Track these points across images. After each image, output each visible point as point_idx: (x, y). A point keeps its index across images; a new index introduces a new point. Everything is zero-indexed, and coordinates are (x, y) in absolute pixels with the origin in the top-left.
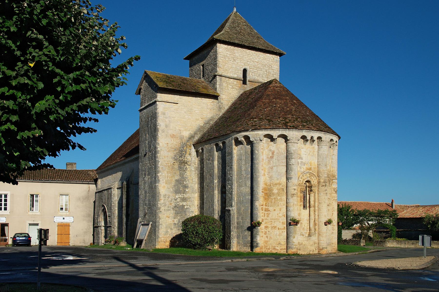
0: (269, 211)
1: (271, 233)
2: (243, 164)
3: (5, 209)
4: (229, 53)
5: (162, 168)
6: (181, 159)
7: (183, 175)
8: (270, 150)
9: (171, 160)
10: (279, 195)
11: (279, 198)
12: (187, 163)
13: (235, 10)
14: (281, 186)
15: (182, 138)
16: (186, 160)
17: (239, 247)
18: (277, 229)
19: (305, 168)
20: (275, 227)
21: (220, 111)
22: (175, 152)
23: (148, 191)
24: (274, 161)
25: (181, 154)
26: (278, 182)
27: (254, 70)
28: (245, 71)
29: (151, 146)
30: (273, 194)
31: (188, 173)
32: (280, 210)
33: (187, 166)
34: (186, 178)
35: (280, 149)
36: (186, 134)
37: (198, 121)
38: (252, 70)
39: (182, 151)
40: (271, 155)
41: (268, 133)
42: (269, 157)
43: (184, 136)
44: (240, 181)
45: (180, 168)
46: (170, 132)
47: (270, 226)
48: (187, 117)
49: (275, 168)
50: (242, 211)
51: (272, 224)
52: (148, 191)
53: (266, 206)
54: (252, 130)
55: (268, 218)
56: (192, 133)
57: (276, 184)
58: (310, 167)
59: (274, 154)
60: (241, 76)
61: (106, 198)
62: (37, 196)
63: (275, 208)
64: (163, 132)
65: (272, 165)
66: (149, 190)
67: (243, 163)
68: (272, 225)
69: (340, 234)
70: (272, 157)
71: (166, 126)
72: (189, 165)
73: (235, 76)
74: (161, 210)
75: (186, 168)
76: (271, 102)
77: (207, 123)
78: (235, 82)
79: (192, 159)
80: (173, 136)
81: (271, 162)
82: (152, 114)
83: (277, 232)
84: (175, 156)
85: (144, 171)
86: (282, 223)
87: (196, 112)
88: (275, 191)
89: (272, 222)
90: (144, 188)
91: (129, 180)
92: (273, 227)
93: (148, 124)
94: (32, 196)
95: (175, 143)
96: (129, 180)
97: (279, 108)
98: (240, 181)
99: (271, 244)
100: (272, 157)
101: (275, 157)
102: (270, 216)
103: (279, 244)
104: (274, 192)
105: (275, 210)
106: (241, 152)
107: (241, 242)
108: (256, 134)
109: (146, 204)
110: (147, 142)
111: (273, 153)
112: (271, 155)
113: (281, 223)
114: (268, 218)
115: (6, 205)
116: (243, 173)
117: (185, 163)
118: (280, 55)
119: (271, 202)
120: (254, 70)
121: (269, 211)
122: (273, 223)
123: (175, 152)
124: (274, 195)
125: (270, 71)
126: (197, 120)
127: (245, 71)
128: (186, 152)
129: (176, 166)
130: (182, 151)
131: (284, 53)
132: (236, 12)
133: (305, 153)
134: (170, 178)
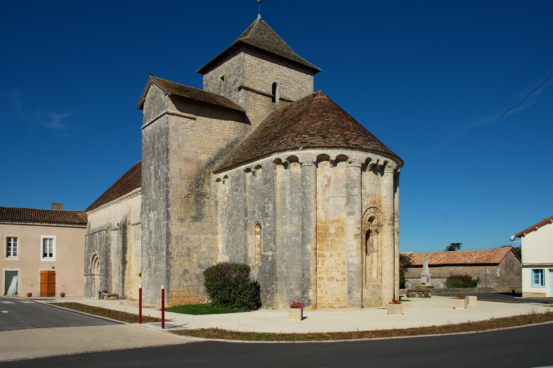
0: (324, 256)
1: (327, 286)
2: (287, 194)
3: (15, 254)
4: (256, 62)
5: (173, 201)
6: (197, 190)
7: (201, 210)
8: (326, 176)
9: (185, 190)
10: (337, 236)
11: (337, 239)
12: (205, 196)
13: (259, 17)
14: (339, 224)
15: (199, 163)
16: (203, 191)
17: (281, 306)
18: (335, 280)
19: (369, 201)
20: (332, 278)
21: (246, 132)
22: (190, 181)
23: (153, 231)
24: (331, 191)
25: (198, 183)
26: (336, 218)
27: (285, 86)
28: (274, 85)
29: (158, 173)
30: (330, 235)
31: (206, 208)
32: (339, 256)
33: (206, 200)
34: (204, 214)
35: (338, 176)
36: (204, 158)
37: (219, 143)
38: (282, 85)
39: (199, 180)
40: (326, 182)
41: (324, 153)
42: (324, 184)
43: (201, 160)
44: (283, 217)
45: (197, 201)
46: (184, 154)
47: (325, 277)
48: (204, 136)
49: (331, 200)
50: (285, 258)
51: (328, 274)
52: (153, 231)
53: (320, 250)
54: (304, 148)
55: (322, 266)
56: (212, 157)
57: (333, 221)
58: (374, 199)
59: (331, 181)
60: (270, 92)
61: (98, 242)
62: (15, 239)
63: (332, 253)
64: (175, 154)
65: (327, 196)
66: (156, 230)
67: (288, 192)
68: (329, 276)
69: (12, 237)
70: (328, 185)
71: (179, 146)
72: (208, 199)
73: (264, 91)
74: (172, 256)
75: (204, 202)
76: (320, 116)
77: (230, 146)
78: (264, 98)
79: (211, 190)
80: (187, 160)
81: (327, 191)
82: (159, 131)
83: (334, 284)
84: (190, 186)
85: (148, 205)
86: (342, 273)
87: (217, 130)
88: (332, 230)
89: (328, 271)
90: (149, 227)
91: (126, 220)
92: (330, 277)
93: (154, 145)
94: (9, 239)
95: (191, 169)
96: (126, 220)
97: (332, 122)
98: (283, 217)
99: (326, 301)
100: (328, 185)
101: (332, 185)
102: (326, 263)
103: (338, 300)
104: (330, 231)
105: (331, 256)
106: (285, 178)
107: (284, 298)
108: (308, 154)
109: (151, 247)
110: (152, 168)
111: (329, 180)
112: (326, 182)
113: (340, 273)
114: (322, 266)
115: (15, 249)
116: (288, 206)
117: (204, 195)
118: (311, 71)
119: (327, 245)
120: (285, 86)
121: (324, 256)
122: (329, 273)
123: (190, 181)
124: (330, 236)
125: (304, 89)
126: (218, 141)
127: (274, 85)
128: (204, 182)
129: (192, 199)
130: (199, 180)
131: (320, 70)
132: (261, 19)
133: (369, 182)
134: (183, 214)
